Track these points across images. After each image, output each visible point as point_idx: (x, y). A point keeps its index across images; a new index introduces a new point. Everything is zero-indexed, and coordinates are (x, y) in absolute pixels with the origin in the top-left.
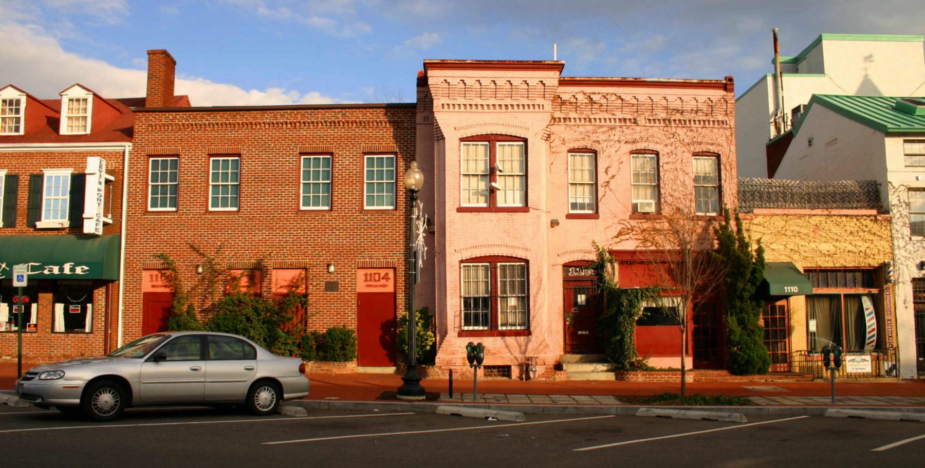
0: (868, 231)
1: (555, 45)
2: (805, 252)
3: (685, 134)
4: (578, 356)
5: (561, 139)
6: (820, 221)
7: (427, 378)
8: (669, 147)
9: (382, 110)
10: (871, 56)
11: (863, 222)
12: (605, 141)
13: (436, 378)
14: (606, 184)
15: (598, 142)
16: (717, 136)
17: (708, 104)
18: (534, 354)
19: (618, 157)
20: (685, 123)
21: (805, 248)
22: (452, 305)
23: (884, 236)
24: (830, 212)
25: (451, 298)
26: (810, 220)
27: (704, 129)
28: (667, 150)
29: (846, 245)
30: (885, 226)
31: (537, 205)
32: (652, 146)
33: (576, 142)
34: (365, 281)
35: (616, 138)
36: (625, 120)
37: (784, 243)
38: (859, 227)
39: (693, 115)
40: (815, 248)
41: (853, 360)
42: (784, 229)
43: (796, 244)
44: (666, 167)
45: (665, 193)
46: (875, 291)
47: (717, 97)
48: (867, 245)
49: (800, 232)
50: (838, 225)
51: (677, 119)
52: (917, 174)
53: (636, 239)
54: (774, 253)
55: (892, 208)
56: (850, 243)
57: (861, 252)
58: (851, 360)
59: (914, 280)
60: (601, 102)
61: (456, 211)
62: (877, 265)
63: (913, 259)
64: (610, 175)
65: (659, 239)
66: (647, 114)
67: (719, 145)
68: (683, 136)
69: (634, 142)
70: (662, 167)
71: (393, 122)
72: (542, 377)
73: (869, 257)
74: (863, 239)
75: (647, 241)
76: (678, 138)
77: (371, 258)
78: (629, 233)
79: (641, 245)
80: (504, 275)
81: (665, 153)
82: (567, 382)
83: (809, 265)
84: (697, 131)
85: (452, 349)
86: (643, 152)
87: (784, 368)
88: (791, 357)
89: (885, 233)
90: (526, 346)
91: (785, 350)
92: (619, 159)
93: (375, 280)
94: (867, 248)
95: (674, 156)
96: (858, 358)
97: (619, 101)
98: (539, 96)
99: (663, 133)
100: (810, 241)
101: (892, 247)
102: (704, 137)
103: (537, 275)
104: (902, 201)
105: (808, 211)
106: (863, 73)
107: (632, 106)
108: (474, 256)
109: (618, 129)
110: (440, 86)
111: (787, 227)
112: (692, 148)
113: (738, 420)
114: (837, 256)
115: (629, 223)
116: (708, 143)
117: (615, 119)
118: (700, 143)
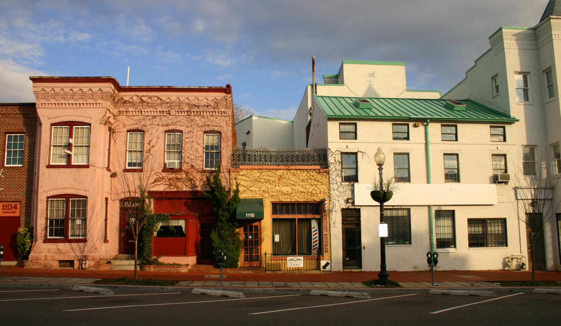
0: (314, 179)
1: (129, 67)
2: (272, 192)
3: (200, 120)
4: (126, 256)
5: (123, 124)
6: (283, 173)
7: (25, 268)
8: (189, 128)
9: (17, 107)
10: (374, 73)
11: (311, 174)
12: (150, 125)
13: (29, 267)
14: (148, 151)
15: (145, 126)
16: (220, 121)
17: (215, 101)
18: (88, 253)
19: (157, 134)
20: (200, 113)
21: (272, 190)
22: (40, 224)
23: (324, 182)
24: (289, 167)
25: (40, 219)
26: (276, 172)
27: (212, 117)
28: (188, 130)
29: (299, 188)
30: (325, 176)
31: (94, 164)
32: (178, 128)
33: (132, 126)
34: (2, 209)
35: (157, 123)
36: (163, 111)
37: (259, 187)
38: (308, 177)
39: (205, 108)
40: (279, 189)
41: (292, 260)
42: (260, 178)
43: (266, 187)
44: (186, 140)
45: (185, 156)
46: (318, 216)
47: (220, 97)
48: (313, 188)
49: (270, 180)
50: (294, 175)
51: (195, 111)
52: (347, 144)
53: (165, 184)
54: (252, 193)
55: (330, 165)
56: (302, 187)
57: (309, 192)
58: (290, 260)
59: (343, 210)
60: (148, 101)
61: (46, 167)
62: (319, 200)
63: (342, 196)
64: (151, 145)
65: (179, 184)
66: (177, 108)
67: (220, 126)
68: (198, 121)
69: (167, 125)
70: (184, 140)
71: (24, 114)
72: (93, 268)
73: (314, 195)
74: (310, 184)
75: (172, 185)
76: (195, 122)
77: (6, 195)
78: (160, 181)
79: (168, 188)
80: (73, 206)
81: (186, 132)
82: (110, 271)
83: (275, 200)
84: (208, 118)
85: (39, 250)
86: (173, 131)
87: (257, 264)
88: (261, 257)
89: (325, 180)
90: (84, 248)
91: (258, 253)
92: (158, 136)
93: (9, 209)
94: (313, 189)
95: (192, 134)
96: (295, 258)
97: (160, 101)
98: (99, 98)
99: (186, 119)
100: (276, 185)
101: (329, 190)
102: (211, 122)
103: (92, 206)
104: (337, 160)
105: (275, 167)
106: (368, 84)
107: (167, 103)
108: (55, 195)
109: (158, 117)
110: (40, 93)
111: (261, 177)
112: (204, 129)
113: (105, 294)
114: (293, 194)
115: (161, 174)
116: (213, 126)
117: (157, 111)
118: (209, 126)
